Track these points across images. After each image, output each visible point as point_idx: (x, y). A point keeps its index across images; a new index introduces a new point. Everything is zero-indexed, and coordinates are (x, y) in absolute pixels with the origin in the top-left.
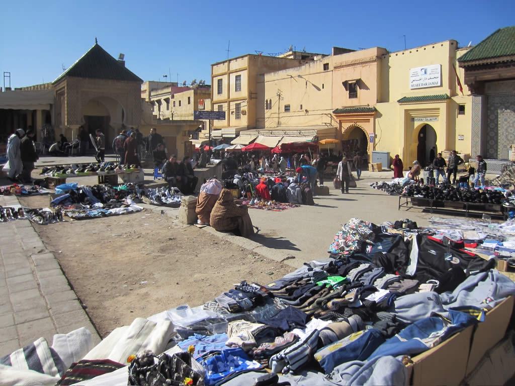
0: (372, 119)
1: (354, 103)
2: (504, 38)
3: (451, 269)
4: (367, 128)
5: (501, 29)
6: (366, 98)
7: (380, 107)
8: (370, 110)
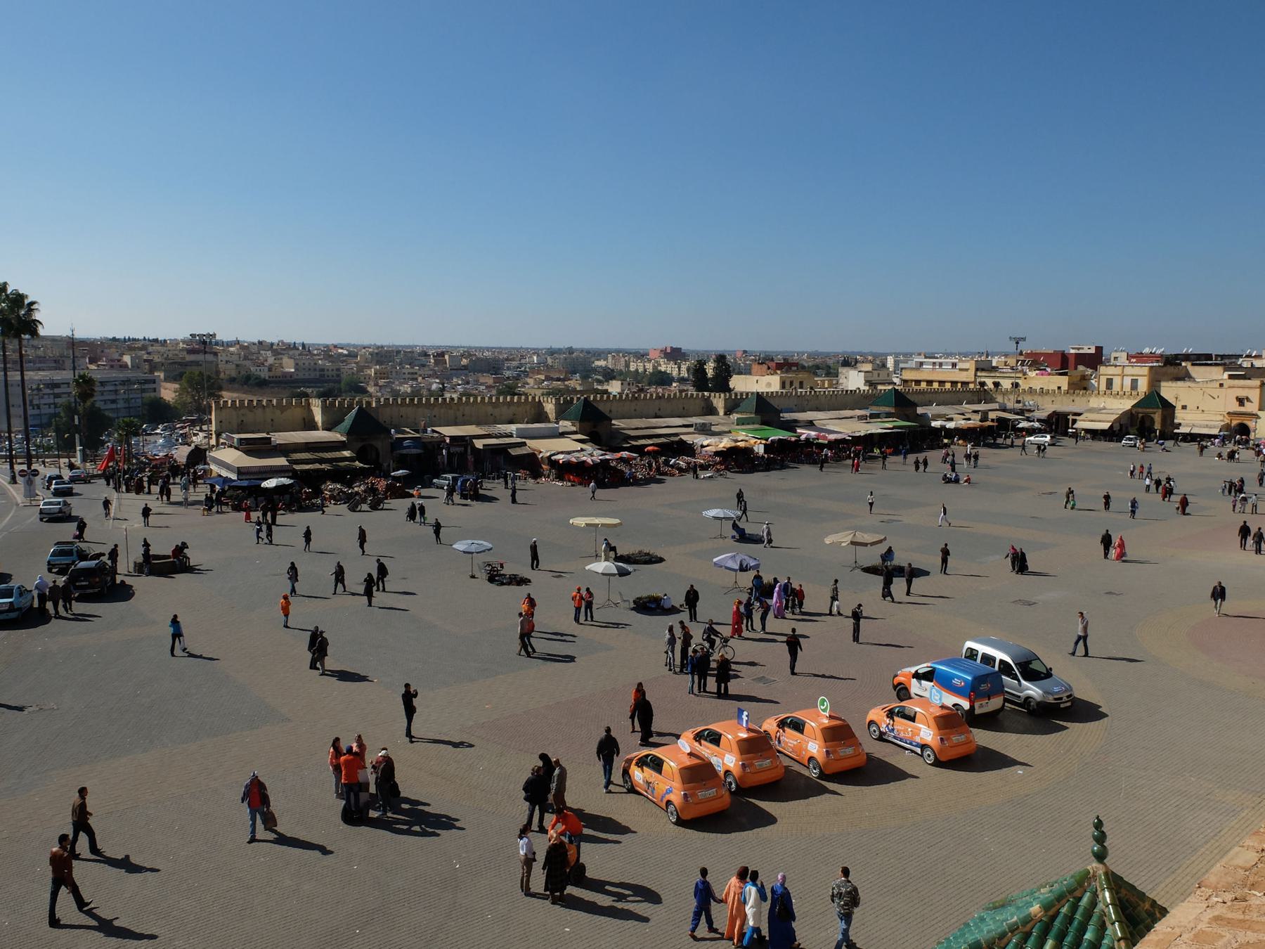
0: (1254, 420)
1: (1242, 409)
2: (1000, 742)
3: (556, 894)
4: (1251, 424)
5: (856, 910)
6: (1251, 407)
7: (1260, 413)
8: (1253, 415)
